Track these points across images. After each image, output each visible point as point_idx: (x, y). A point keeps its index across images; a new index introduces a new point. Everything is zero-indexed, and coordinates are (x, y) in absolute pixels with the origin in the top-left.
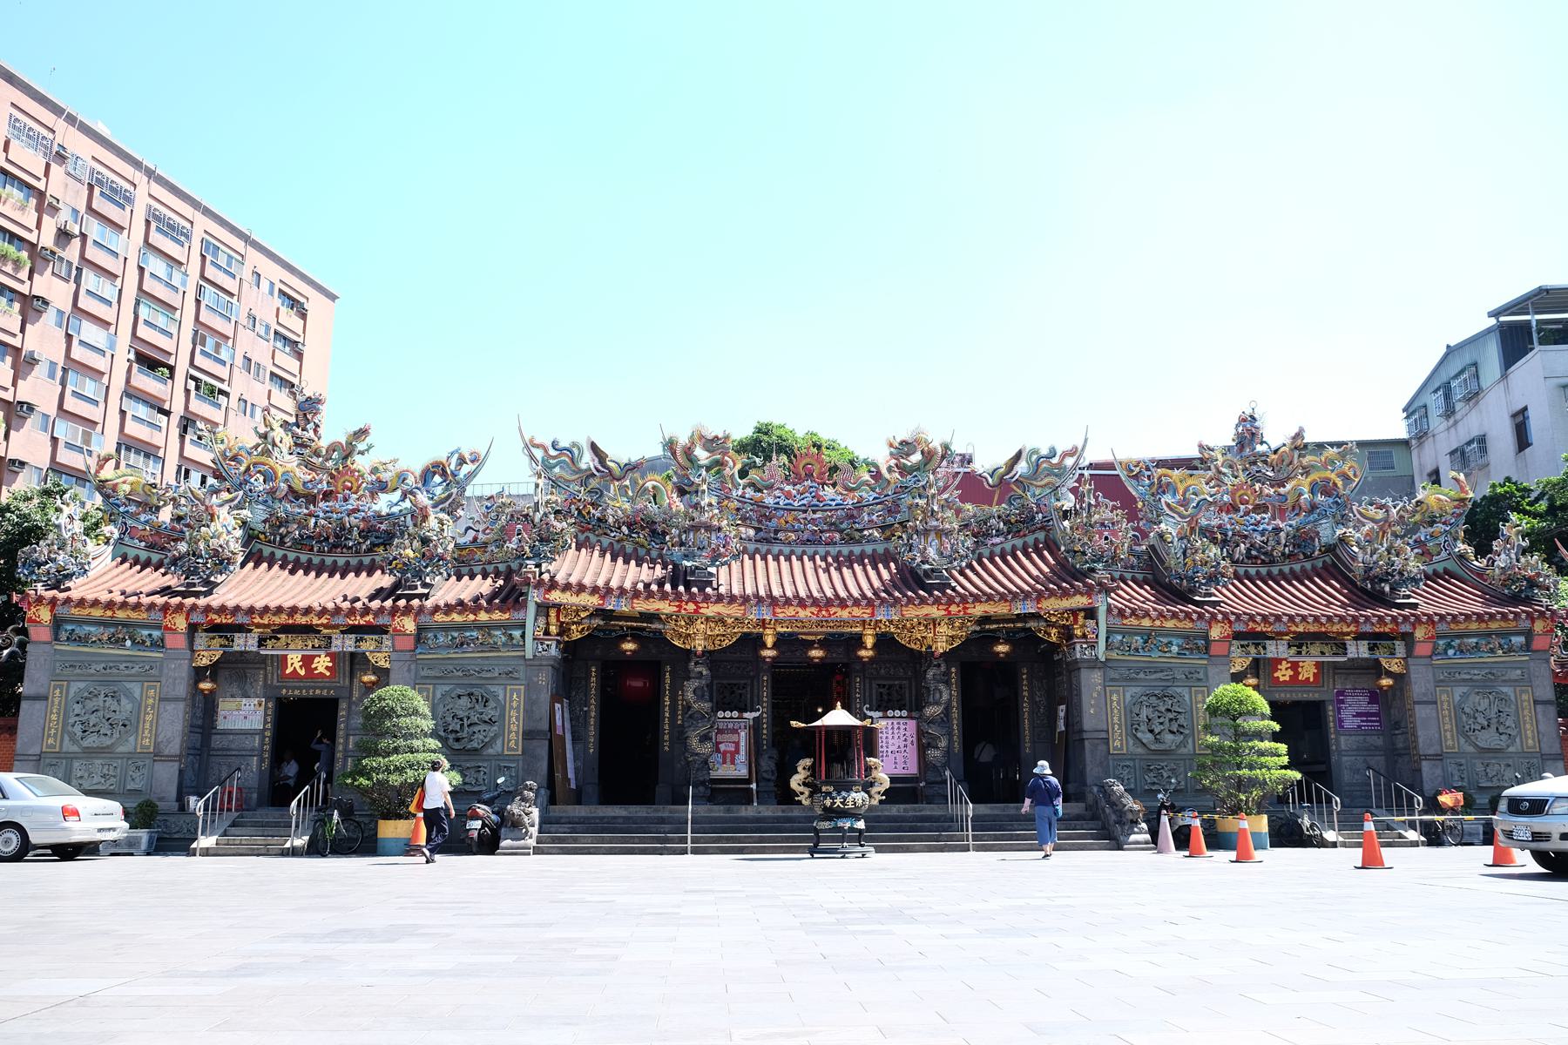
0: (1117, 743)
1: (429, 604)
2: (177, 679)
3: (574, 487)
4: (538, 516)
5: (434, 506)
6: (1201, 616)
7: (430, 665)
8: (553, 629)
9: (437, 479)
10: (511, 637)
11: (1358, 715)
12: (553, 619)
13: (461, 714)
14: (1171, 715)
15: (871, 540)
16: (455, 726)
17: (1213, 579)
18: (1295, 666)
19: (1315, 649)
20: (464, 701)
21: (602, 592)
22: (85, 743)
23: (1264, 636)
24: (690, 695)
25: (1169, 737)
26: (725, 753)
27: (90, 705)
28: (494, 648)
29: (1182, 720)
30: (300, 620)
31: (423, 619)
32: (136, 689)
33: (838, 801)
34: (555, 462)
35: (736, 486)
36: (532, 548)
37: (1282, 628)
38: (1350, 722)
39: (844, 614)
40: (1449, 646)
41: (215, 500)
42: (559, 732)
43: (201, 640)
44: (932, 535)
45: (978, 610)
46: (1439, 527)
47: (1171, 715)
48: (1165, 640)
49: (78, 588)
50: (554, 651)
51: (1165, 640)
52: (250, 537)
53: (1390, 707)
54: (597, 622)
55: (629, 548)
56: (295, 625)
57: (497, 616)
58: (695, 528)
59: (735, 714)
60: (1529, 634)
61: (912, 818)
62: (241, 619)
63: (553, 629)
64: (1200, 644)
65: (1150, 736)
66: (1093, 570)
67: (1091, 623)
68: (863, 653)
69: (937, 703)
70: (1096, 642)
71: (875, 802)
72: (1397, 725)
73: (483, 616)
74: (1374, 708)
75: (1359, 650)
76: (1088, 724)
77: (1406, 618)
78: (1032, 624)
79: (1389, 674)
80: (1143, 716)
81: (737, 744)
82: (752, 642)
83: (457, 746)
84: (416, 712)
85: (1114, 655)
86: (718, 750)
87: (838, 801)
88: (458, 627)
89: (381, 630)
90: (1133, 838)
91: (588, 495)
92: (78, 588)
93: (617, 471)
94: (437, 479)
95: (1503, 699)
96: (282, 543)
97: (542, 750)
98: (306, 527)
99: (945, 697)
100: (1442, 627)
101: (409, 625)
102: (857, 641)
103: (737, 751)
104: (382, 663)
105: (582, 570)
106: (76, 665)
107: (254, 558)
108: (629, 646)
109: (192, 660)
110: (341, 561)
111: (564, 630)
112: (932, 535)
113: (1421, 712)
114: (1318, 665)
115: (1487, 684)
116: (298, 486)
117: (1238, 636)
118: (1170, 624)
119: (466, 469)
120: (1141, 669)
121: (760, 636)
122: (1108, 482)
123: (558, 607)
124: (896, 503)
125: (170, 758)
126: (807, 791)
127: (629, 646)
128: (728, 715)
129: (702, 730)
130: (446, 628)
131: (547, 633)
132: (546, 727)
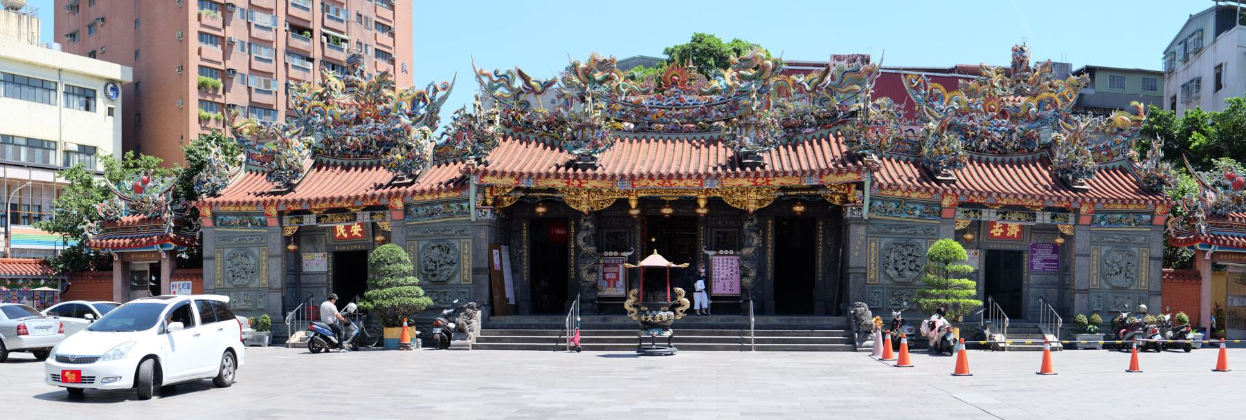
0: (872, 276)
1: (417, 187)
2: (276, 241)
3: (510, 102)
4: (477, 126)
5: (414, 124)
6: (937, 190)
7: (414, 228)
8: (489, 201)
9: (421, 104)
10: (462, 208)
11: (1044, 261)
12: (488, 195)
13: (434, 259)
14: (911, 258)
15: (718, 129)
16: (431, 266)
17: (953, 164)
18: (1005, 227)
19: (1014, 216)
20: (436, 251)
21: (517, 175)
22: (235, 283)
23: (981, 206)
24: (581, 242)
25: (908, 273)
26: (609, 280)
27: (235, 261)
28: (451, 215)
29: (918, 262)
30: (338, 205)
31: (407, 200)
32: (256, 251)
33: (650, 317)
34: (492, 84)
35: (621, 94)
36: (473, 148)
37: (992, 201)
38: (1038, 265)
39: (682, 184)
40: (1103, 219)
41: (287, 134)
42: (497, 268)
43: (286, 220)
44: (753, 127)
45: (777, 182)
46: (1120, 138)
47: (911, 258)
48: (911, 206)
49: (226, 195)
50: (489, 216)
51: (911, 206)
52: (315, 153)
53: (1062, 257)
54: (520, 194)
55: (548, 140)
56: (339, 209)
57: (452, 195)
58: (582, 127)
59: (616, 253)
60: (1152, 214)
61: (723, 323)
62: (305, 207)
63: (489, 201)
64: (934, 209)
65: (895, 272)
66: (865, 155)
67: (860, 192)
68: (699, 211)
69: (750, 246)
70: (862, 207)
71: (678, 318)
72: (1067, 269)
73: (443, 195)
74: (1055, 257)
75: (1044, 218)
76: (852, 263)
77: (1076, 199)
78: (821, 192)
79: (1063, 235)
80: (892, 258)
81: (617, 274)
82: (623, 204)
83: (434, 279)
84: (399, 261)
85: (874, 215)
86: (604, 278)
87: (650, 317)
88: (434, 205)
89: (384, 208)
90: (865, 343)
91: (521, 110)
92: (226, 195)
93: (539, 89)
94: (421, 104)
95: (1131, 255)
96: (333, 154)
97: (485, 282)
98: (345, 143)
99: (756, 242)
100: (1098, 206)
101: (399, 204)
102: (694, 202)
103: (617, 279)
104: (387, 228)
105: (519, 160)
106: (225, 238)
107: (318, 165)
108: (541, 210)
109: (283, 232)
110: (368, 162)
111: (497, 201)
112: (753, 127)
113: (1079, 262)
114: (1020, 227)
115: (1123, 245)
116: (338, 118)
117: (961, 205)
118: (914, 195)
119: (440, 94)
120: (893, 226)
121: (627, 200)
122: (890, 83)
123: (491, 187)
124: (736, 103)
125: (276, 290)
126: (636, 311)
127: (541, 210)
128: (611, 253)
129: (589, 265)
130: (422, 204)
131: (485, 204)
132: (486, 265)
